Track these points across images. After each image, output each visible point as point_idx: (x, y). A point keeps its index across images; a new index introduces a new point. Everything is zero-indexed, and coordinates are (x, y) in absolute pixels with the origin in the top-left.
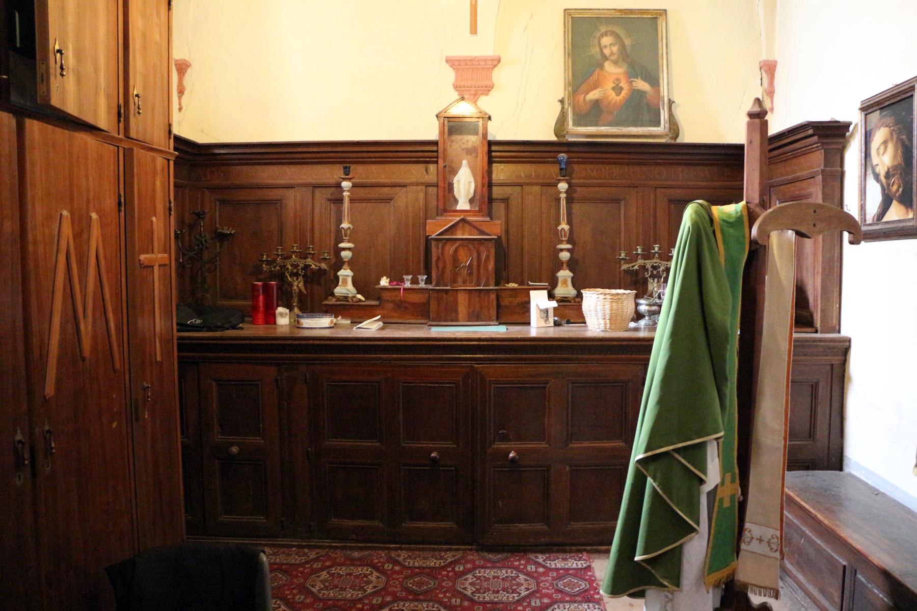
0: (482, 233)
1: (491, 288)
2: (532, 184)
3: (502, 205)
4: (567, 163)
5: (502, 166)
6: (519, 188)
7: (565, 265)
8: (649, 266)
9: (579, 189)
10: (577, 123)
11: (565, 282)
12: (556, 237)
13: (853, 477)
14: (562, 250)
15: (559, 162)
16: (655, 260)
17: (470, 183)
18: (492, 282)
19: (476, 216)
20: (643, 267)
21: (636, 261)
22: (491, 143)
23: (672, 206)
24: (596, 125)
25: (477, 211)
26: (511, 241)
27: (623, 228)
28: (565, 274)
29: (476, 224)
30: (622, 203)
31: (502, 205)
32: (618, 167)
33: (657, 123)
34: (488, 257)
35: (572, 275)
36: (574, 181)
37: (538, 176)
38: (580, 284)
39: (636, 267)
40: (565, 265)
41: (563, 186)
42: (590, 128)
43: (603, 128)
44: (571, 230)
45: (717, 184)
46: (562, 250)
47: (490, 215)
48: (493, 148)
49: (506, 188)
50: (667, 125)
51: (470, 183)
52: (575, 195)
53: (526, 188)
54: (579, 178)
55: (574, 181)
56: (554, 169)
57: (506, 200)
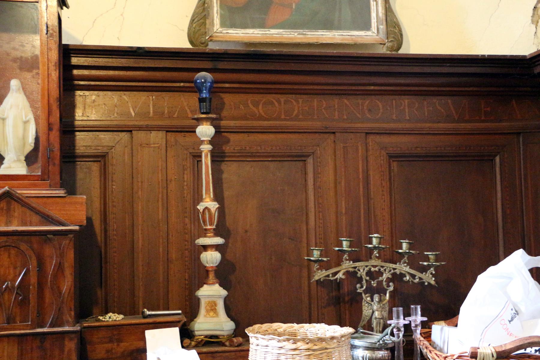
0: (48, 219)
1: (67, 328)
2: (149, 129)
3: (95, 167)
4: (212, 91)
5: (92, 96)
6: (125, 136)
7: (211, 276)
8: (362, 273)
9: (233, 137)
10: (229, 21)
11: (212, 307)
12: (195, 222)
13: (74, 169)
14: (205, 248)
15: (198, 89)
16: (373, 262)
17: (26, 122)
18: (69, 316)
19: (35, 186)
20: (352, 275)
21: (338, 264)
22: (67, 52)
23: (395, 165)
24: (262, 25)
25: (37, 178)
26: (111, 233)
27: (311, 204)
28: (211, 292)
29: (34, 203)
30: (310, 160)
31: (95, 167)
32: (301, 99)
33: (367, 26)
34: (60, 267)
35: (224, 293)
36: (223, 123)
37: (160, 114)
38: (245, 313)
39: (340, 275)
40: (211, 276)
41: (205, 131)
42: (250, 31)
43: (273, 31)
44: (221, 210)
45: (469, 126)
46: (205, 248)
47: (71, 191)
48: (75, 61)
49: (102, 135)
50: (382, 27)
51: (26, 122)
52: (227, 149)
53: (140, 136)
54: (234, 118)
55: (223, 123)
56: (188, 102)
57: (101, 158)
